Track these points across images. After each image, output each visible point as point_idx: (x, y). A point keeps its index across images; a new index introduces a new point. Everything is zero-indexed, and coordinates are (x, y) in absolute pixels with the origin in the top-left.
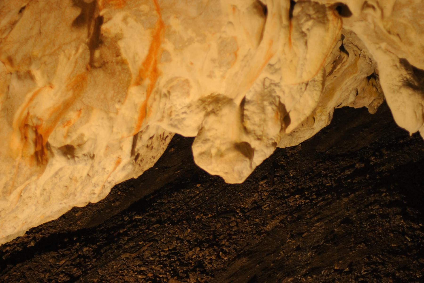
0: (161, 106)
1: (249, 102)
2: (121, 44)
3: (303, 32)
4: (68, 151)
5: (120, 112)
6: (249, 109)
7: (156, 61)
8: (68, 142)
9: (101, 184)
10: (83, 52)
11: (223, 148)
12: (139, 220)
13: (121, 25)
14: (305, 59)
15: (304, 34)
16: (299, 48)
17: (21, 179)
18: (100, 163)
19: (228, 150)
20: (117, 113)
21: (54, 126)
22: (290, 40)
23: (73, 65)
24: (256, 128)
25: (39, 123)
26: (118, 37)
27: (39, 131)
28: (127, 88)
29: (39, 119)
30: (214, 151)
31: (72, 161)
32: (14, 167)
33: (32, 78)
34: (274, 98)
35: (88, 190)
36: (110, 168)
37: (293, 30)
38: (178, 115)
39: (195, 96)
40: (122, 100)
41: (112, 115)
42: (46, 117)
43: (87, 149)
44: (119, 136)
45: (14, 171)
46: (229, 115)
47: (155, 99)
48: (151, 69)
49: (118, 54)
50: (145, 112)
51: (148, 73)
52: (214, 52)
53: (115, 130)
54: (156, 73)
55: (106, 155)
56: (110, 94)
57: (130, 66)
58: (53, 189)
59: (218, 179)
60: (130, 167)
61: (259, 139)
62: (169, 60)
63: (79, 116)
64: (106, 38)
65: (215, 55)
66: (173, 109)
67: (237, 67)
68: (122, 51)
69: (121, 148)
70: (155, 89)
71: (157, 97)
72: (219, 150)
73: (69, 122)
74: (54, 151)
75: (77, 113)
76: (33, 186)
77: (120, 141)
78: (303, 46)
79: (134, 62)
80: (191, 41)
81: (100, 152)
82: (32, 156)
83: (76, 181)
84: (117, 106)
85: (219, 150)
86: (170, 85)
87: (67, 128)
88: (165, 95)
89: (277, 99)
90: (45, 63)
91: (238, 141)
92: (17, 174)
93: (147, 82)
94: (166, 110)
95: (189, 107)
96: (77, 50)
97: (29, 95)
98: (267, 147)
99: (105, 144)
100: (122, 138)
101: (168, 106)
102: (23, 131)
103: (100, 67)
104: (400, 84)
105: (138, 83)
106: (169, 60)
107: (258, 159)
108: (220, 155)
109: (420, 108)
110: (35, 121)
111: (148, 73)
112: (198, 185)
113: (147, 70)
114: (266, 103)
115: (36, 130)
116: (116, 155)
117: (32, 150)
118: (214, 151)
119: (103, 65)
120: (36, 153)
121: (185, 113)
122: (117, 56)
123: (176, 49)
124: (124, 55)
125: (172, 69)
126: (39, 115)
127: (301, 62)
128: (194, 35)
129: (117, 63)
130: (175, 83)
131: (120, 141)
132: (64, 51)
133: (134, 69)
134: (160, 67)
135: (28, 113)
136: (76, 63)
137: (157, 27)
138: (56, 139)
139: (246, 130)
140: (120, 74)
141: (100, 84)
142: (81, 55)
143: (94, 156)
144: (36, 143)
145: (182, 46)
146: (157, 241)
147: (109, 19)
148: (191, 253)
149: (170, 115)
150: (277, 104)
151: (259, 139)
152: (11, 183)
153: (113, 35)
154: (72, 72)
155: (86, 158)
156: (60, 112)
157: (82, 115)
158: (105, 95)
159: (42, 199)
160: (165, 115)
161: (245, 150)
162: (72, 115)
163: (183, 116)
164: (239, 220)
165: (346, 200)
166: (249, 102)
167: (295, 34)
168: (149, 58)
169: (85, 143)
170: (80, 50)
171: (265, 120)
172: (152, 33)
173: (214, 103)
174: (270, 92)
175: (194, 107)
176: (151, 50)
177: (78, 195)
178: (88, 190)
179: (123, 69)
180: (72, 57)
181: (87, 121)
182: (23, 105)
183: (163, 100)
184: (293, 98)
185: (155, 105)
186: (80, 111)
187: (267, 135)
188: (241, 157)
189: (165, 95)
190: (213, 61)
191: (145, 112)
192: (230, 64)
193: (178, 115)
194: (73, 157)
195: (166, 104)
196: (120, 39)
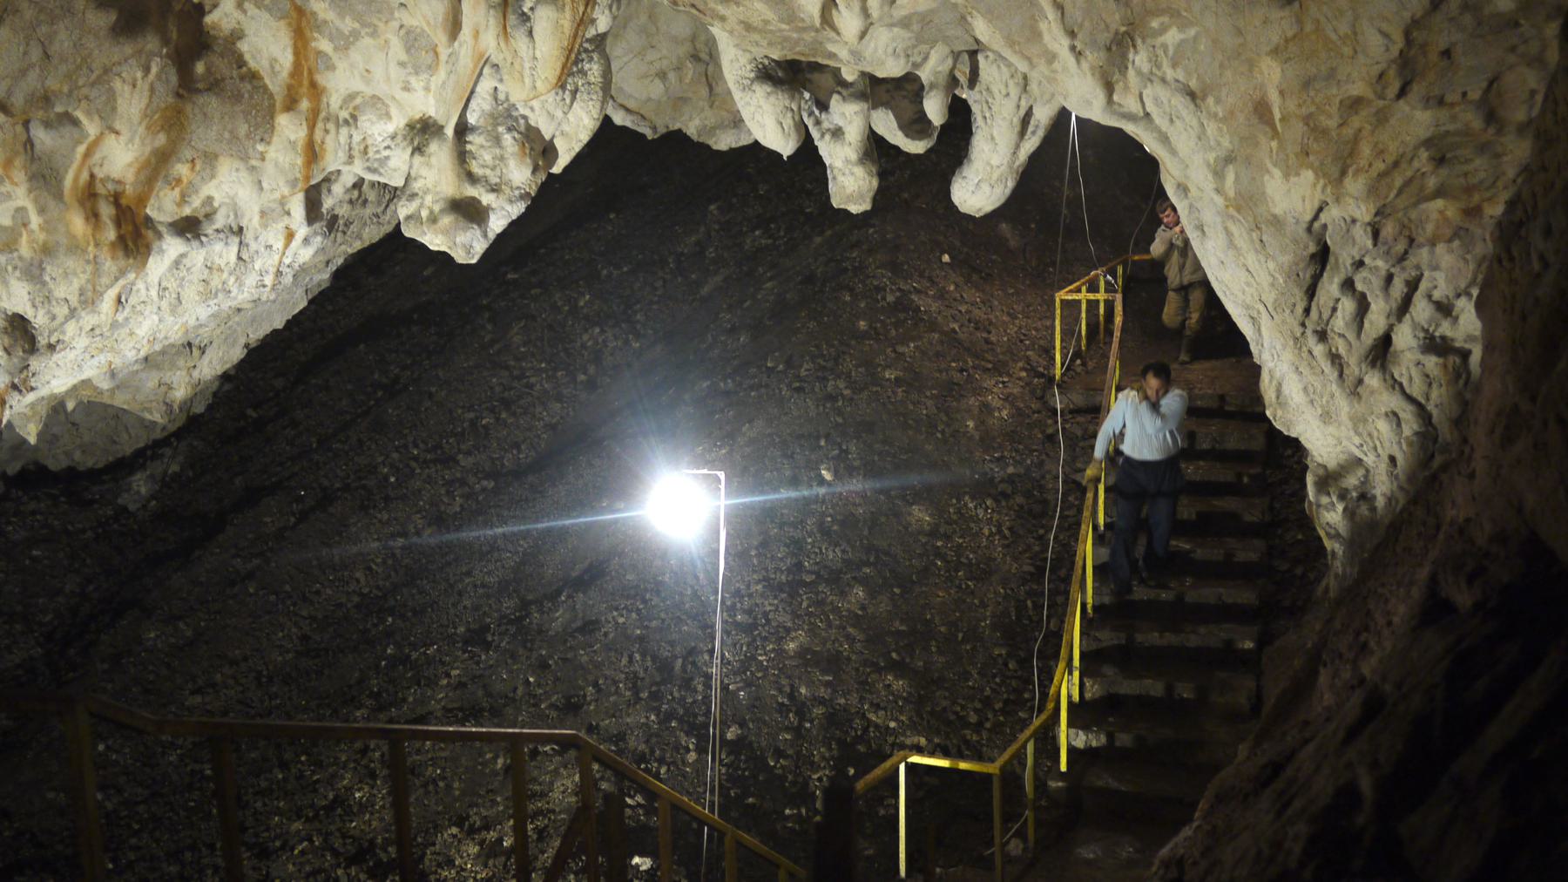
0: (343, 139)
1: (473, 129)
2: (243, 46)
3: (524, 14)
4: (189, 228)
5: (268, 156)
6: (475, 141)
7: (310, 72)
8: (187, 211)
9: (273, 270)
10: (162, 70)
11: (437, 208)
12: (515, 281)
13: (237, 14)
14: (535, 58)
15: (525, 18)
16: (521, 42)
17: (105, 280)
18: (256, 238)
19: (442, 211)
20: (263, 159)
21: (151, 189)
22: (505, 27)
23: (147, 94)
24: (488, 172)
25: (119, 188)
26: (237, 35)
27: (124, 202)
28: (272, 118)
29: (119, 182)
30: (424, 214)
31: (195, 243)
32: (88, 262)
33: (75, 123)
34: (516, 120)
35: (251, 280)
36: (279, 245)
37: (510, 10)
38: (378, 152)
39: (398, 122)
40: (266, 136)
41: (254, 162)
42: (130, 177)
43: (220, 221)
44: (277, 195)
45: (89, 268)
46: (441, 153)
47: (327, 131)
48: (306, 83)
49: (241, 62)
50: (312, 153)
51: (304, 90)
52: (397, 50)
53: (265, 185)
54: (316, 91)
55: (265, 226)
56: (243, 129)
57: (267, 81)
58: (181, 286)
59: (444, 257)
60: (319, 239)
61: (493, 190)
62: (332, 68)
63: (193, 169)
64: (215, 38)
65: (404, 57)
66: (369, 142)
67: (442, 73)
68: (247, 57)
69: (288, 214)
70: (323, 115)
71: (331, 126)
72: (432, 212)
73: (179, 181)
74: (162, 229)
75: (189, 165)
76: (140, 285)
77: (282, 202)
78: (526, 40)
79: (274, 73)
80: (355, 35)
81: (251, 220)
82: (113, 245)
83: (220, 270)
84: (260, 147)
85: (432, 212)
86: (352, 105)
87: (177, 190)
88: (346, 122)
89: (522, 121)
90: (87, 98)
91: (458, 197)
92: (97, 273)
93: (305, 104)
94: (354, 145)
95: (393, 138)
96: (147, 70)
97: (81, 149)
98: (511, 202)
99: (256, 209)
100: (283, 197)
101: (357, 138)
102: (88, 205)
103: (209, 90)
104: (752, 75)
105: (291, 105)
106: (332, 68)
107: (497, 224)
108: (433, 219)
109: (789, 115)
110: (110, 186)
111: (304, 90)
112: (612, 216)
113: (300, 85)
114: (501, 129)
115: (116, 199)
116: (281, 226)
117: (111, 234)
118: (424, 214)
119: (215, 85)
120: (121, 238)
121: (388, 147)
122: (240, 67)
123: (336, 49)
124: (252, 64)
125: (340, 83)
126: (115, 175)
127: (527, 65)
128: (357, 25)
129: (242, 78)
130: (358, 101)
131: (282, 202)
132: (119, 75)
133: (276, 84)
134: (321, 79)
135: (92, 176)
136: (152, 90)
137: (294, 15)
138: (163, 207)
139: (472, 178)
140: (251, 97)
141: (210, 123)
142: (158, 77)
143: (241, 229)
144: (118, 224)
145: (346, 43)
146: (533, 318)
147: (215, 6)
148: (585, 337)
149: (365, 152)
150: (522, 129)
151: (495, 189)
152: (90, 287)
153: (227, 32)
154: (148, 106)
155: (222, 235)
156: (157, 166)
157: (198, 168)
158: (231, 132)
159: (164, 304)
160: (356, 153)
161: (468, 211)
162: (182, 170)
163: (386, 153)
164: (668, 277)
165: (818, 240)
166: (473, 129)
167: (512, 19)
168: (297, 65)
169: (215, 212)
170: (154, 70)
171: (502, 158)
172: (290, 24)
173: (422, 131)
174: (508, 110)
175: (399, 137)
176: (296, 53)
177: (235, 291)
178: (251, 280)
179: (254, 87)
180: (139, 82)
181: (213, 177)
182: (75, 166)
183: (344, 131)
184: (552, 117)
185: (329, 140)
186: (193, 161)
187: (508, 183)
188: (462, 222)
189: (346, 122)
190: (402, 64)
191: (312, 153)
192: (432, 68)
193: (378, 152)
194: (197, 236)
195: (351, 137)
196: (240, 38)
